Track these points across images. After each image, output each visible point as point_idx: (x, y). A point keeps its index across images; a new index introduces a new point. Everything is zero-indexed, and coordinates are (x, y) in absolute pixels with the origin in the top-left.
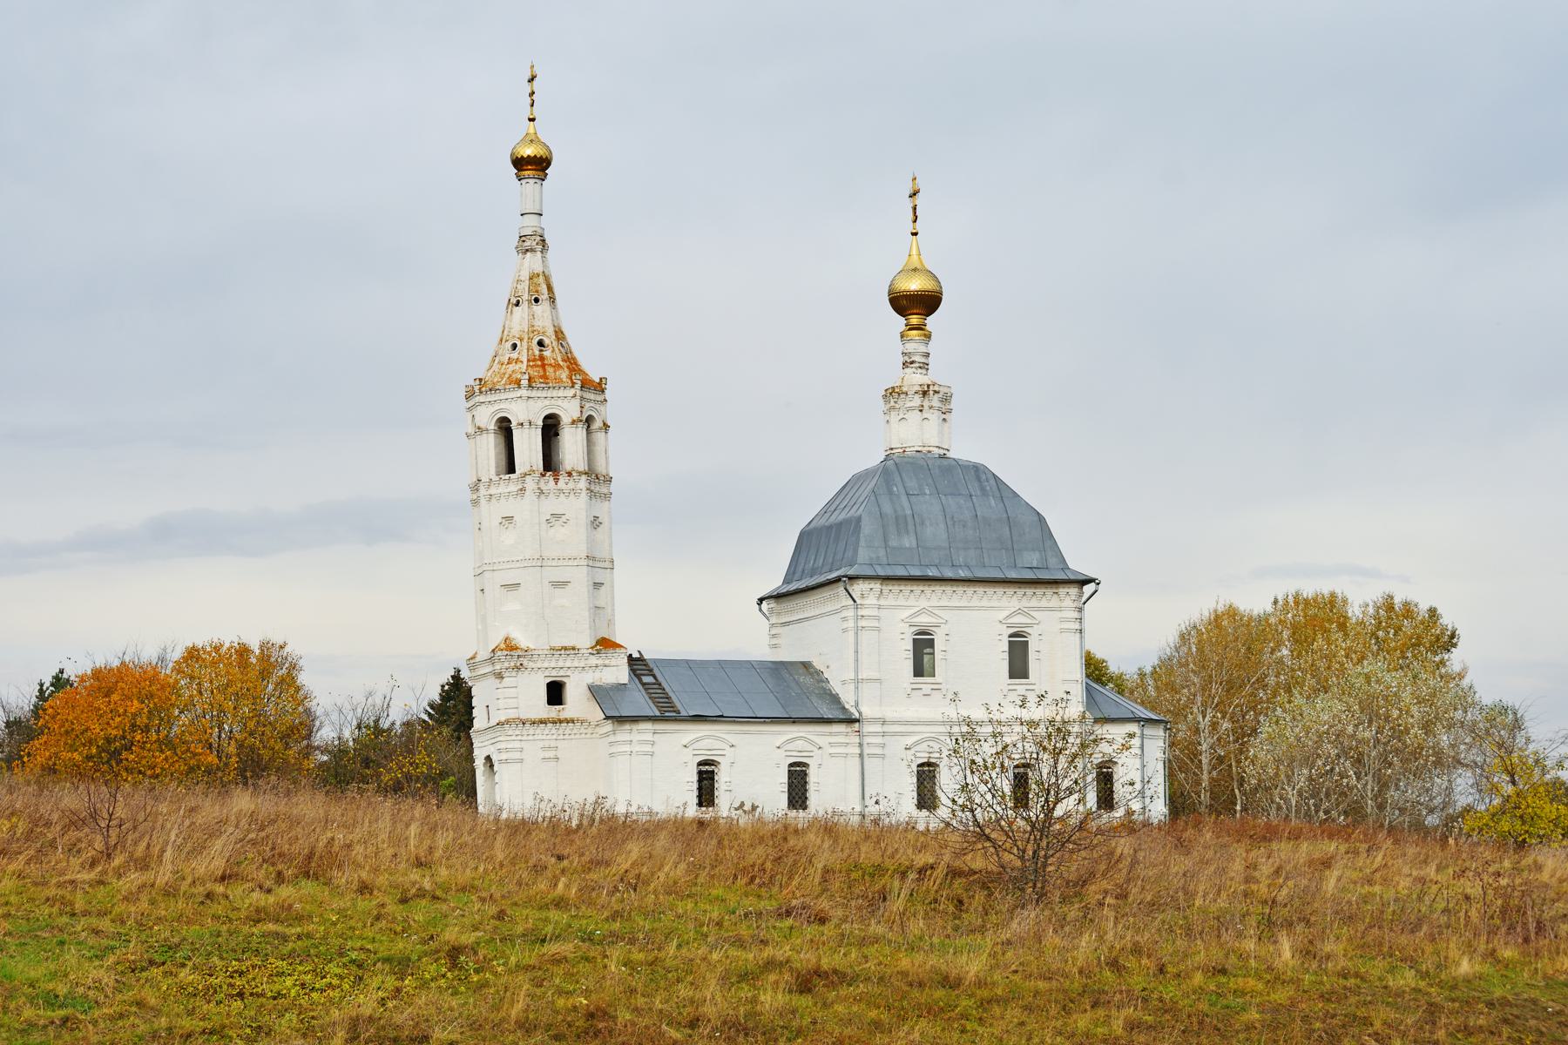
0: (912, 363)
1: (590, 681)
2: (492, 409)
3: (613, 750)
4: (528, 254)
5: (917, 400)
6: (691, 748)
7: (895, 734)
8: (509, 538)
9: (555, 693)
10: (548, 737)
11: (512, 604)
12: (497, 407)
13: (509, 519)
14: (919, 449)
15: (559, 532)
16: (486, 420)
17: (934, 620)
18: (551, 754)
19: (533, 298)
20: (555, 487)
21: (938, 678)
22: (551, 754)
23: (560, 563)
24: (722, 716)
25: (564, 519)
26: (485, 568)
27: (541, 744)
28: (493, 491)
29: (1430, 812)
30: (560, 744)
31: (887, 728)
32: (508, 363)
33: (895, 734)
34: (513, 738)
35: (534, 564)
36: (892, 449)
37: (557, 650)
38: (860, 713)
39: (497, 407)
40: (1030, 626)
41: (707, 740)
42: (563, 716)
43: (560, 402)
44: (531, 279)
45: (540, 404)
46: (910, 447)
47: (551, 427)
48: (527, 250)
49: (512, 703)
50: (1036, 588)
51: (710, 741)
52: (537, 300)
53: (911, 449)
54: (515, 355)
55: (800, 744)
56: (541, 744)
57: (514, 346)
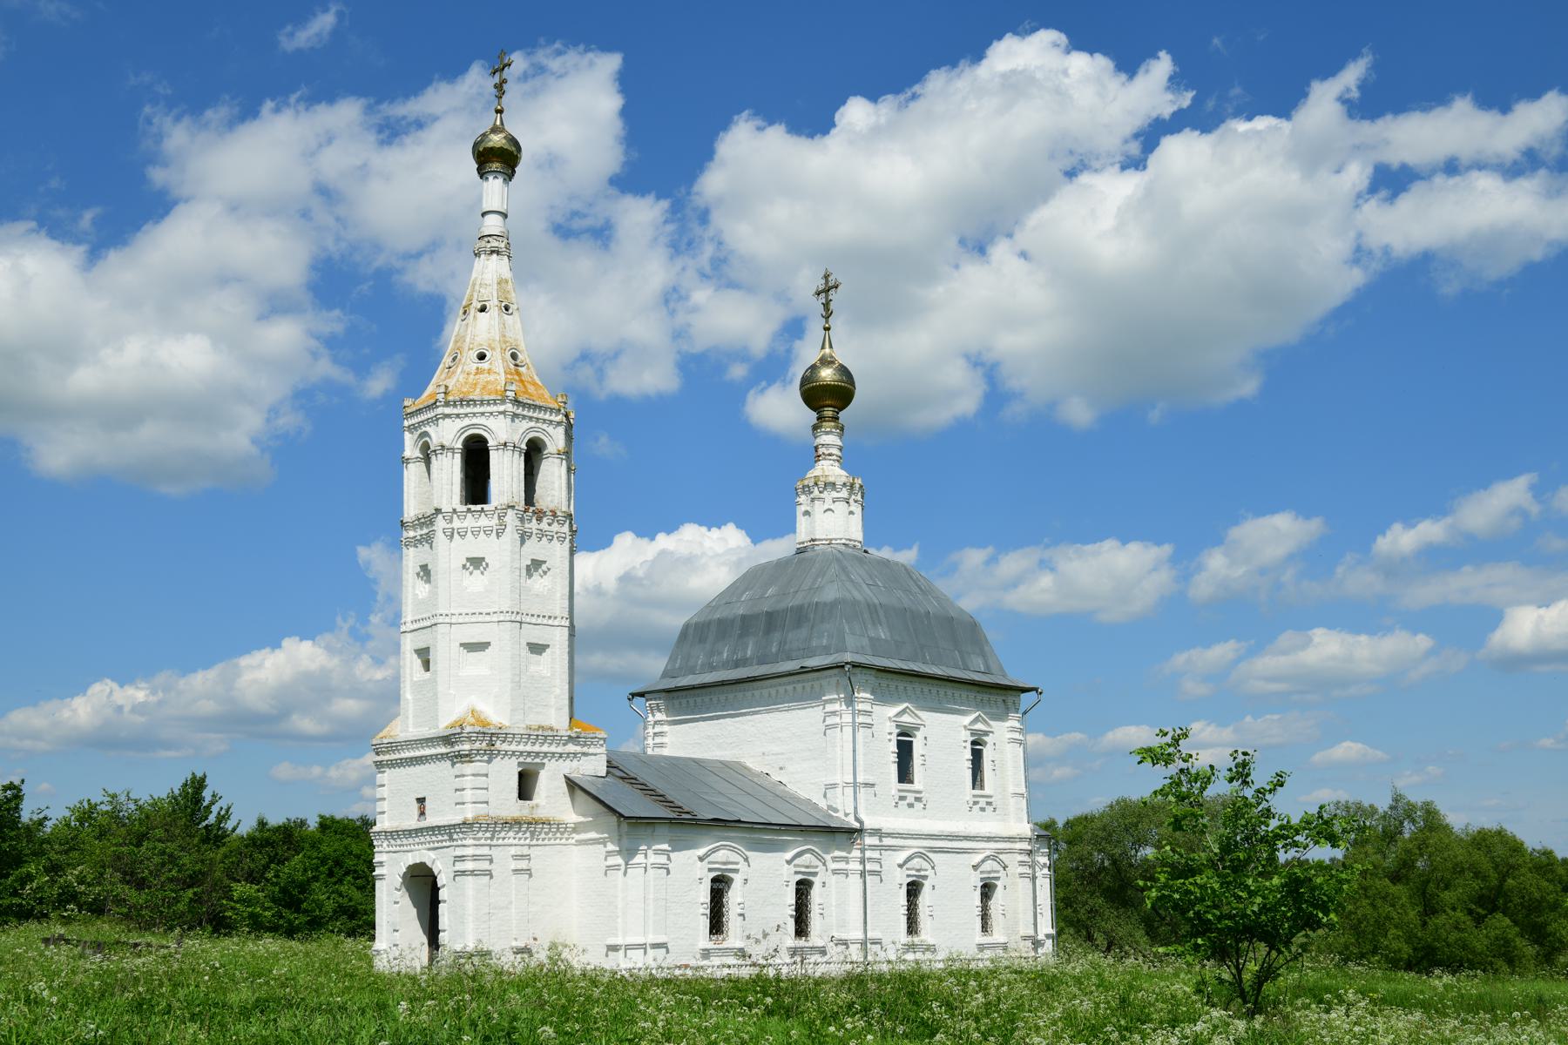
0: (830, 455)
1: (566, 772)
2: (460, 424)
3: (460, 866)
4: (495, 255)
5: (844, 493)
6: (706, 860)
7: (890, 848)
8: (476, 582)
9: (526, 785)
10: (522, 842)
11: (476, 665)
12: (467, 422)
13: (476, 562)
14: (847, 542)
15: (539, 583)
16: (452, 437)
17: (914, 721)
18: (523, 864)
19: (503, 304)
20: (538, 527)
21: (917, 786)
22: (523, 864)
23: (539, 621)
24: (739, 821)
25: (544, 567)
26: (440, 620)
27: (513, 851)
28: (457, 524)
29: (169, 929)
30: (534, 852)
31: (887, 841)
32: (476, 374)
33: (890, 848)
34: (483, 842)
35: (513, 619)
36: (813, 540)
37: (534, 729)
38: (861, 823)
39: (467, 422)
40: (986, 733)
41: (722, 851)
42: (912, 789)
43: (550, 429)
44: (499, 283)
45: (526, 424)
46: (836, 540)
47: (533, 453)
48: (492, 252)
49: (481, 795)
50: (990, 694)
51: (726, 851)
52: (507, 308)
53: (838, 542)
54: (485, 365)
55: (722, 855)
56: (513, 851)
57: (482, 357)
